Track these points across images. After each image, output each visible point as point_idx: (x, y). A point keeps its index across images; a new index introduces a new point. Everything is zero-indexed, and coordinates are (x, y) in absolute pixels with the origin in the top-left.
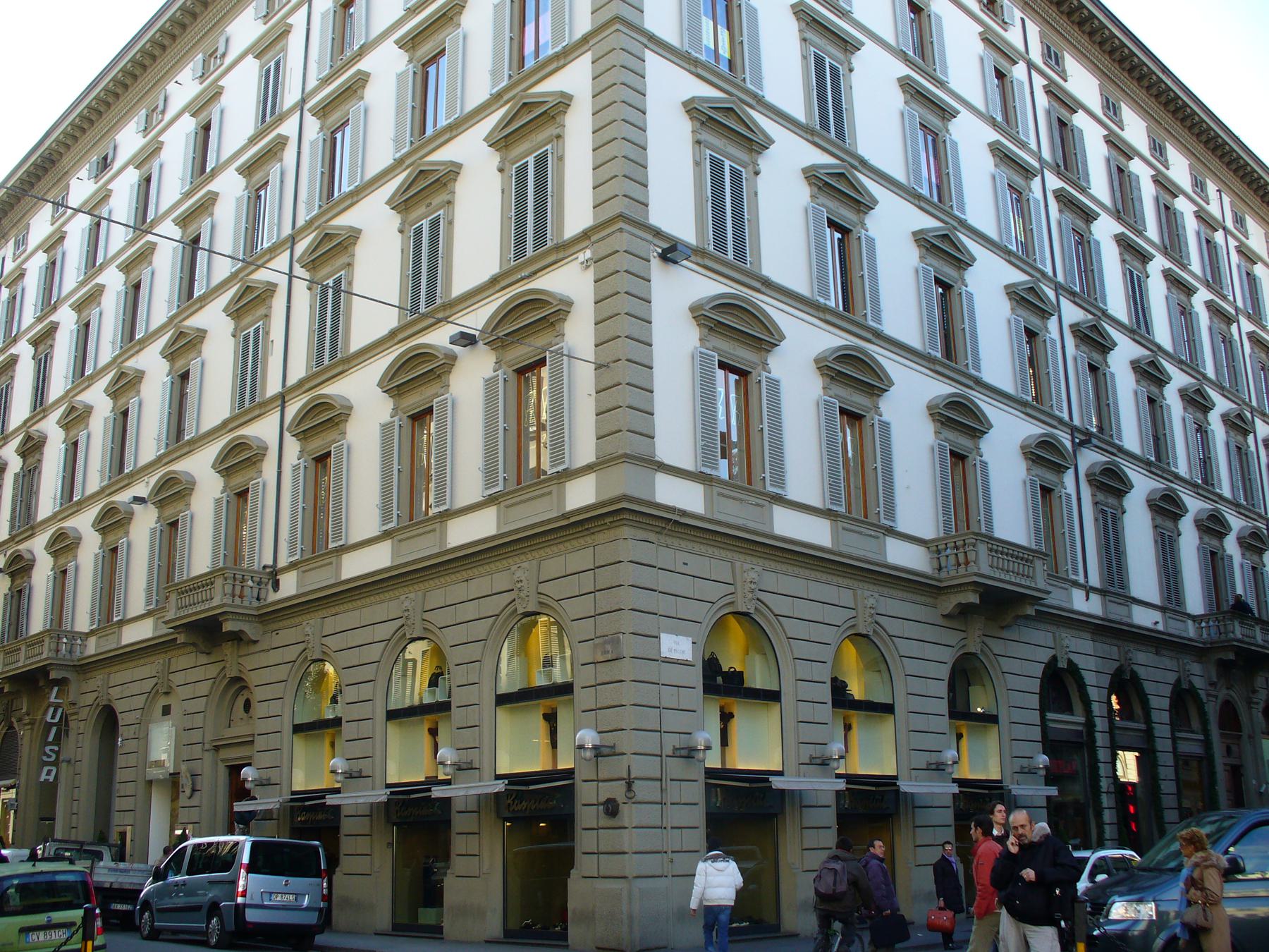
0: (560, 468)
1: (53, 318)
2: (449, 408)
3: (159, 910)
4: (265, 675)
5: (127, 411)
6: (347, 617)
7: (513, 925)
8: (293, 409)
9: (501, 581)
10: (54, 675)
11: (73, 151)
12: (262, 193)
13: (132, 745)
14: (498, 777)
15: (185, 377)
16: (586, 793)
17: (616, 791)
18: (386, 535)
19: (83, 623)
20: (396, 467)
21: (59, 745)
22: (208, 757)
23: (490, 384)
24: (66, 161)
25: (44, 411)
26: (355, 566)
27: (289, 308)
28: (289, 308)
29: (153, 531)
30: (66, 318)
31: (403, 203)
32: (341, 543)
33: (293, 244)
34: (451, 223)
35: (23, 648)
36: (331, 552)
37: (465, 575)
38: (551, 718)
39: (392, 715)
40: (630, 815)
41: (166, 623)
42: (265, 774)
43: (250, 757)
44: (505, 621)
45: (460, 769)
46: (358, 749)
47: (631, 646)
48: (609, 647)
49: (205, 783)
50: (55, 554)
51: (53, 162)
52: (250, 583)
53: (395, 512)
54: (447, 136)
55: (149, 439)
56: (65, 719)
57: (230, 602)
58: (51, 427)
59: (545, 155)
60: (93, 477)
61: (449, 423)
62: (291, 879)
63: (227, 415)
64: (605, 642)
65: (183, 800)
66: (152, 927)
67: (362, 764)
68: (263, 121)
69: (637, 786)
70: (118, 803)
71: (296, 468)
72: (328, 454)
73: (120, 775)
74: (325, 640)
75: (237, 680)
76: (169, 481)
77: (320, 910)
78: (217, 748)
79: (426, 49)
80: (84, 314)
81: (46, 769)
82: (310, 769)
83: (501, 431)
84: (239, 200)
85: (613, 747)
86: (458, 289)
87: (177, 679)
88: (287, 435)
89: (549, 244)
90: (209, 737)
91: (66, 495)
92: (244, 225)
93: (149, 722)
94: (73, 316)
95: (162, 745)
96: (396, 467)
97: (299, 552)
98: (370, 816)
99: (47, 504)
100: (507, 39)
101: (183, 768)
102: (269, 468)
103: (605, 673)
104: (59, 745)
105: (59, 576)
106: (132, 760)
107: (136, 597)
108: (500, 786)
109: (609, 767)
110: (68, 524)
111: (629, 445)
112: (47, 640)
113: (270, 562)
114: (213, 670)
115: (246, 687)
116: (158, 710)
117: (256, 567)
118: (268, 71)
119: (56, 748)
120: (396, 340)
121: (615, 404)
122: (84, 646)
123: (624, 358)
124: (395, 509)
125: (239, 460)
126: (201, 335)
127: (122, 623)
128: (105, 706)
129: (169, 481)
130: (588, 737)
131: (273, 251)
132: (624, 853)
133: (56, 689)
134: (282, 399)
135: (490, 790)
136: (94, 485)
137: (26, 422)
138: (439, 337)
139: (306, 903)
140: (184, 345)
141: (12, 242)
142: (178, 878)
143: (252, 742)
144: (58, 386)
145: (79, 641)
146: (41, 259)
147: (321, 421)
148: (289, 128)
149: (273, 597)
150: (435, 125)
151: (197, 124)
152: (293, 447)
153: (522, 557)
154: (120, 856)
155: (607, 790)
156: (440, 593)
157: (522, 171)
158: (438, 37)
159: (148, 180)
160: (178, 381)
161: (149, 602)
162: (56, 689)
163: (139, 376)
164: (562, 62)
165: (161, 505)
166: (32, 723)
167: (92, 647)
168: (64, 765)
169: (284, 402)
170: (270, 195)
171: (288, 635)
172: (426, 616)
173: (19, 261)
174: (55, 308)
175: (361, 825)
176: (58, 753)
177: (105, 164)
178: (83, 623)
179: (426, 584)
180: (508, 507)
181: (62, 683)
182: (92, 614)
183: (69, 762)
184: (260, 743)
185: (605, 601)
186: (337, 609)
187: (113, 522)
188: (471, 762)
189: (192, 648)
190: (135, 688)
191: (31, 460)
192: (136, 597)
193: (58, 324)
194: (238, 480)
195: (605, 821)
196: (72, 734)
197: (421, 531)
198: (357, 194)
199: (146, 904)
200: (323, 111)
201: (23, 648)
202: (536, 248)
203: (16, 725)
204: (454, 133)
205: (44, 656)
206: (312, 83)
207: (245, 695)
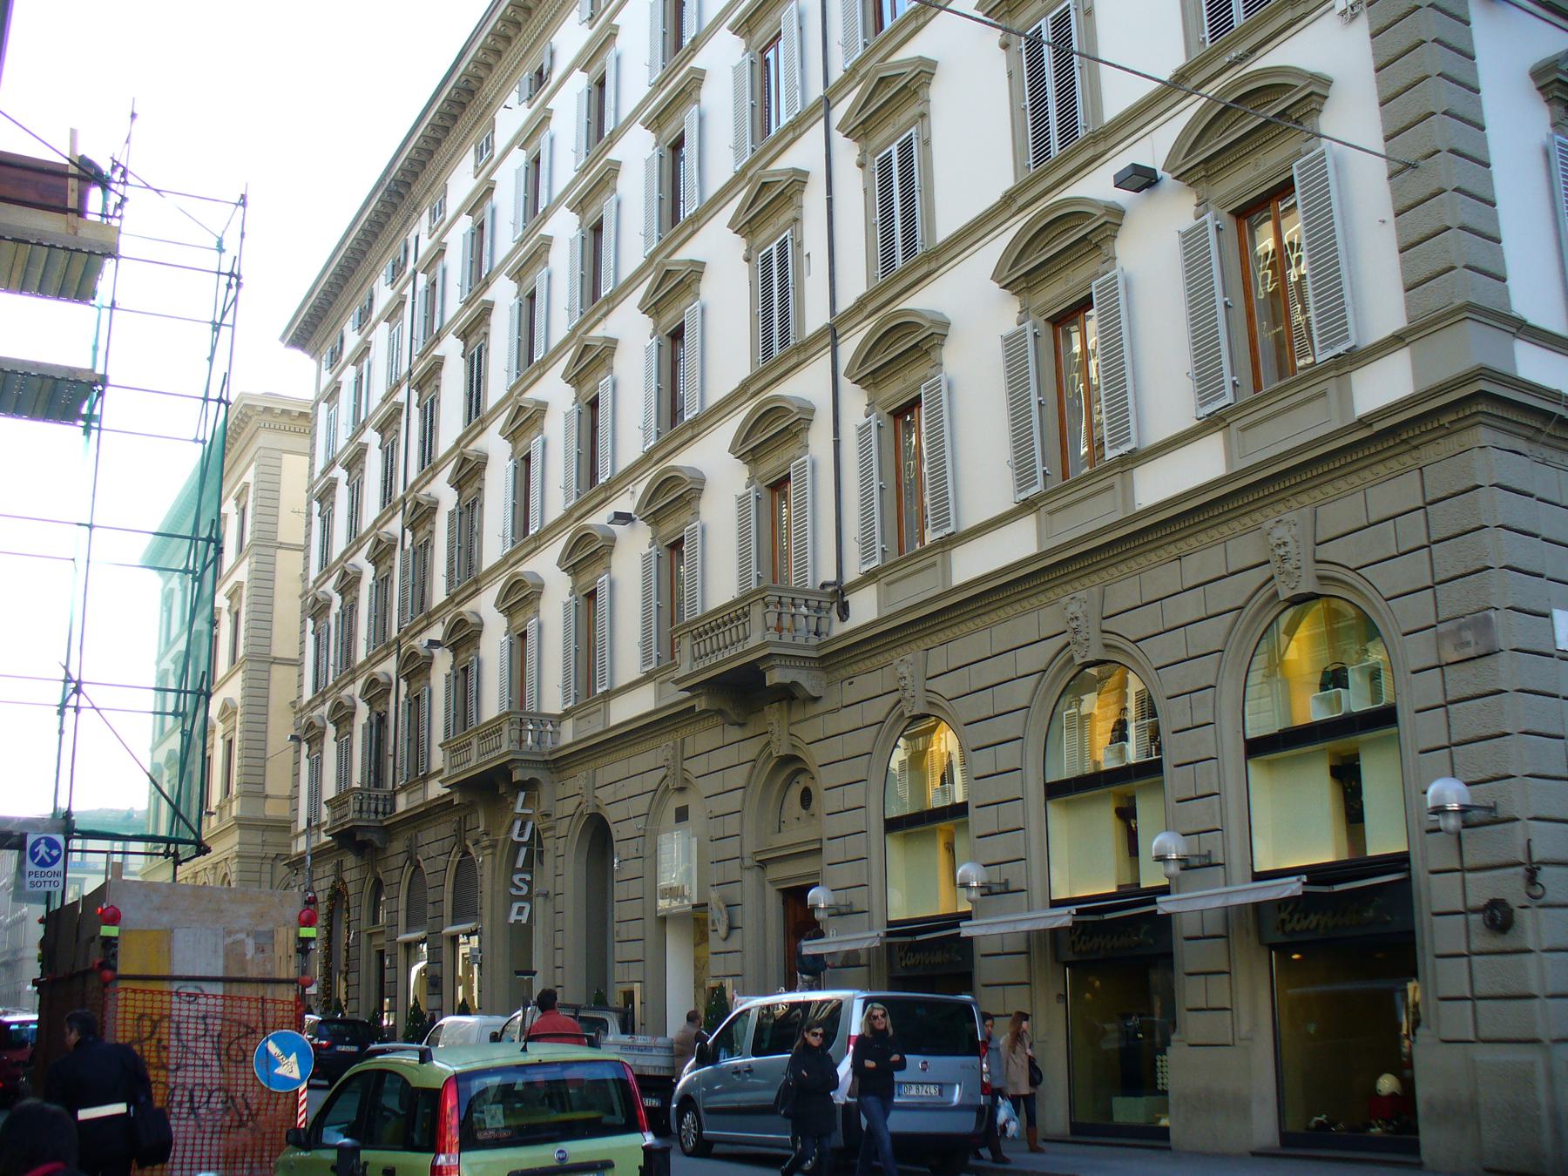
0: (1340, 349)
1: (487, 296)
2: (1121, 290)
3: (710, 1111)
4: (835, 749)
5: (681, 328)
6: (970, 643)
7: (1293, 1126)
8: (849, 346)
9: (1244, 550)
10: (518, 776)
11: (498, 71)
12: (771, 55)
13: (634, 868)
14: (1055, 904)
15: (677, 335)
16: (1437, 893)
17: (1510, 887)
18: (1026, 507)
19: (553, 700)
20: (1034, 399)
21: (531, 872)
22: (750, 878)
23: (1191, 241)
24: (488, 89)
25: (482, 421)
26: (971, 564)
27: (830, 201)
28: (830, 201)
29: (646, 559)
30: (504, 293)
31: (747, 226)
32: (948, 530)
34: (927, 143)
35: (475, 742)
36: (1112, 465)
37: (1173, 550)
38: (1126, 814)
39: (1054, 791)
40: (1535, 926)
41: (677, 682)
42: (842, 898)
43: (817, 874)
44: (891, 728)
45: (991, 893)
46: (999, 848)
47: (1510, 630)
48: (1468, 636)
49: (747, 917)
50: (509, 612)
51: (472, 93)
52: (804, 610)
53: (1039, 470)
55: (631, 430)
56: (537, 837)
57: (775, 638)
58: (495, 445)
60: (555, 497)
61: (1123, 313)
62: (930, 1059)
64: (1460, 628)
65: (715, 942)
66: (699, 1136)
67: (1211, 843)
69: (1546, 875)
70: (621, 951)
71: (863, 431)
72: (787, 478)
73: (620, 911)
74: (932, 685)
75: (791, 759)
76: (667, 482)
77: (980, 1110)
78: (763, 864)
80: (528, 281)
81: (516, 906)
82: (915, 887)
83: (1220, 309)
84: (737, 70)
85: (1492, 809)
86: (945, 229)
87: (696, 767)
88: (845, 383)
89: (1081, 133)
90: (750, 848)
91: (520, 526)
93: (657, 833)
94: (512, 287)
95: (677, 863)
96: (1034, 399)
97: (878, 554)
98: (1027, 953)
99: (493, 548)
100: (748, 107)
101: (714, 896)
102: (819, 440)
103: (1462, 681)
104: (531, 872)
105: (517, 641)
106: (635, 889)
107: (628, 653)
108: (1064, 918)
109: (1480, 847)
110: (524, 568)
112: (506, 728)
113: (832, 577)
114: (751, 749)
115: (804, 771)
116: (671, 814)
117: (810, 585)
119: (528, 878)
120: (1014, 208)
121: (1437, 225)
122: (556, 734)
123: (1444, 148)
124: (1038, 462)
125: (772, 434)
126: (697, 270)
127: (609, 695)
128: (591, 815)
129: (667, 482)
130: (1449, 791)
131: (798, 126)
132: (1532, 997)
133: (522, 795)
134: (832, 333)
135: (1042, 925)
136: (556, 509)
137: (458, 442)
138: (1097, 185)
139: (956, 1098)
140: (672, 288)
141: (426, 216)
142: (737, 1061)
144: (497, 386)
145: (549, 727)
146: (466, 223)
147: (900, 352)
149: (839, 628)
150: (778, 123)
151: (590, 80)
152: (855, 402)
153: (1076, 584)
154: (627, 1026)
155: (1482, 889)
156: (1125, 586)
157: (885, 164)
159: (537, 161)
160: (667, 343)
161: (646, 660)
162: (522, 795)
163: (542, 408)
164: (921, 20)
165: (655, 519)
166: (493, 846)
167: (568, 734)
168: (539, 901)
169: (835, 338)
170: (784, 55)
171: (869, 681)
172: (1107, 625)
174: (487, 284)
175: (1015, 968)
176: (530, 884)
177: (540, 78)
178: (553, 700)
179: (1103, 574)
180: (1244, 429)
181: (530, 786)
182: (566, 687)
183: (546, 895)
184: (832, 851)
185: (1449, 559)
186: (949, 634)
187: (587, 555)
188: (1209, 855)
189: (718, 719)
190: (634, 786)
191: (469, 491)
192: (628, 653)
193: (492, 303)
194: (771, 466)
195: (1482, 941)
196: (548, 858)
197: (1257, 416)
199: (687, 1101)
201: (475, 742)
202: (1063, 145)
203: (472, 850)
205: (504, 749)
207: (803, 781)
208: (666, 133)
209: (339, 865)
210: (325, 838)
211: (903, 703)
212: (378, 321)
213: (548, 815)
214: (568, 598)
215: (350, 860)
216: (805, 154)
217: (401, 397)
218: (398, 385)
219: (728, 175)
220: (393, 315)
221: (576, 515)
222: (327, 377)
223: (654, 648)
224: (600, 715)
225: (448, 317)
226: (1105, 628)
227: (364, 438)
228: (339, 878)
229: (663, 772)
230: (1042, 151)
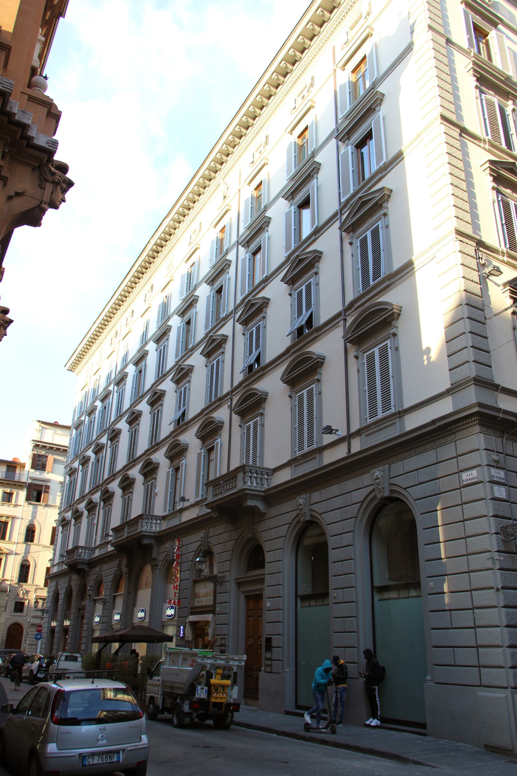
59: (310, 284)
63: (203, 406)
79: (253, 246)
94: (134, 368)
120: (353, 309)
127: (402, 413)
143: (263, 579)
157: (300, 294)
158: (258, 240)
172: (392, 481)
180: (366, 436)
198: (266, 281)
200: (247, 243)
204: (384, 173)
208: (215, 286)
209: (70, 578)
210: (110, 548)
211: (300, 516)
215: (75, 577)
216: (226, 330)
217: (111, 388)
218: (110, 383)
223: (168, 506)
224: (105, 548)
226: (391, 482)
229: (200, 542)
230: (152, 443)
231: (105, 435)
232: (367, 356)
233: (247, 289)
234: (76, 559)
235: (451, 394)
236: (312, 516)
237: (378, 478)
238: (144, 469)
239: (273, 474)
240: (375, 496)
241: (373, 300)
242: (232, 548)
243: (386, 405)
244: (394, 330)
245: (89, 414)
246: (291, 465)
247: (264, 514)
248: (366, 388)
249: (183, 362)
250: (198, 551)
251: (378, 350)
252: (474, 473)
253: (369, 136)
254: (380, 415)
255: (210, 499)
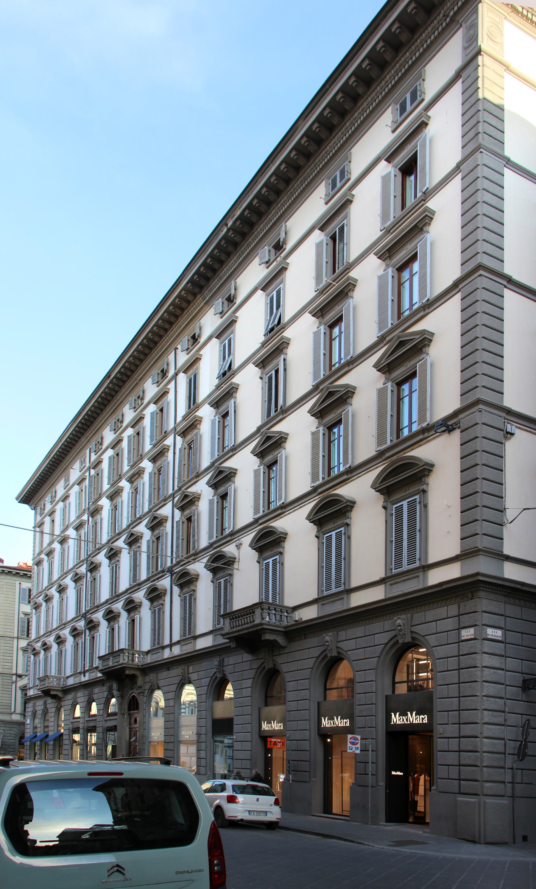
30: (206, 413)
33: (174, 498)
54: (346, 369)
68: (190, 407)
79: (331, 316)
92: (76, 549)
111: (189, 634)
118: (272, 299)
127: (196, 638)
148: (169, 441)
158: (337, 309)
173: (66, 489)
192: (204, 620)
204: (351, 367)
206: (179, 419)
212: (210, 338)
213: (141, 687)
214: (56, 651)
219: (373, 339)
220: (80, 482)
221: (152, 579)
222: (39, 518)
224: (78, 678)
225: (71, 521)
227: (53, 546)
228: (34, 709)
231: (41, 595)
232: (395, 508)
233: (322, 373)
234: (47, 687)
235: (460, 560)
236: (338, 653)
237: (400, 626)
238: (257, 541)
239: (293, 612)
240: (326, 655)
241: (329, 491)
242: (252, 677)
243: (411, 560)
244: (424, 487)
245: (92, 514)
246: (385, 583)
247: (284, 648)
248: (394, 539)
249: (187, 489)
250: (214, 677)
251: (407, 504)
252: (472, 631)
253: (340, 320)
254: (405, 567)
255: (227, 629)
